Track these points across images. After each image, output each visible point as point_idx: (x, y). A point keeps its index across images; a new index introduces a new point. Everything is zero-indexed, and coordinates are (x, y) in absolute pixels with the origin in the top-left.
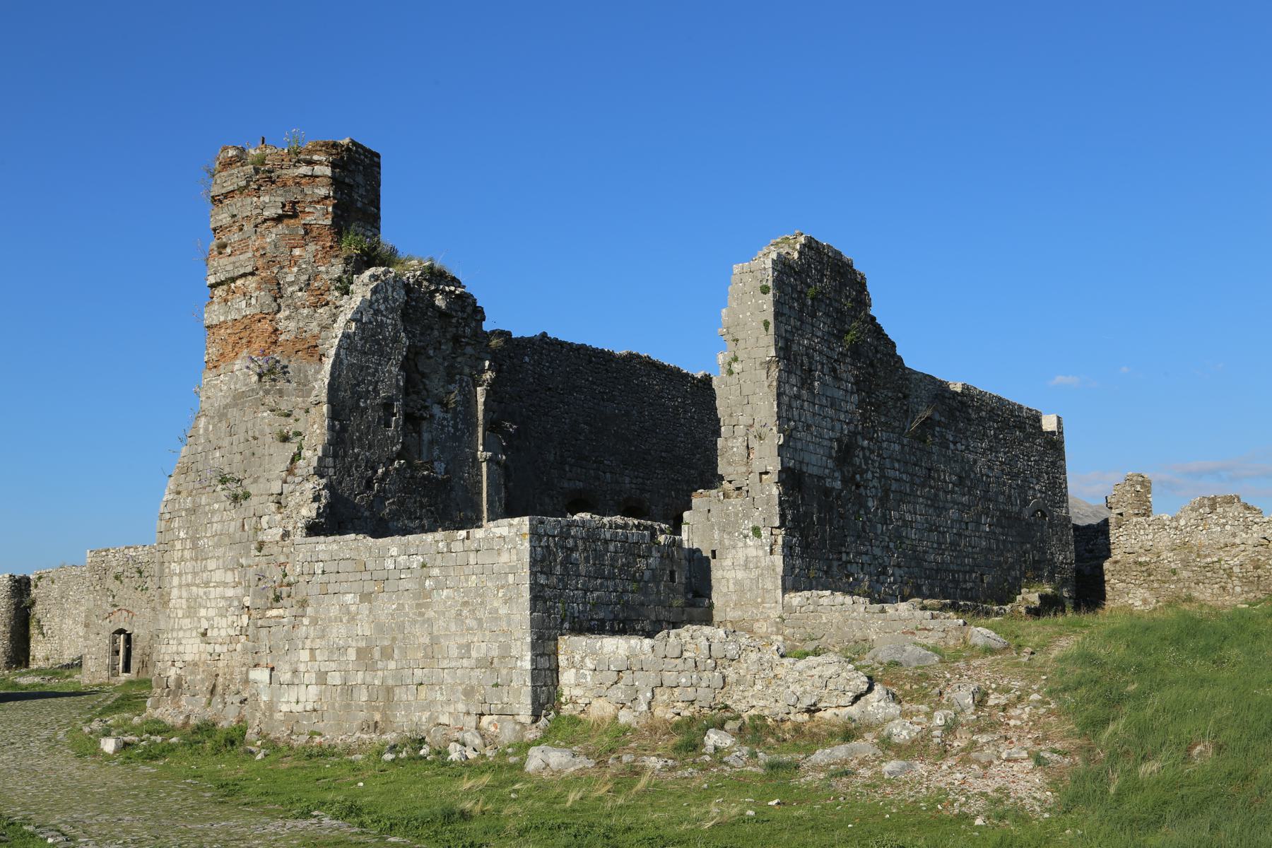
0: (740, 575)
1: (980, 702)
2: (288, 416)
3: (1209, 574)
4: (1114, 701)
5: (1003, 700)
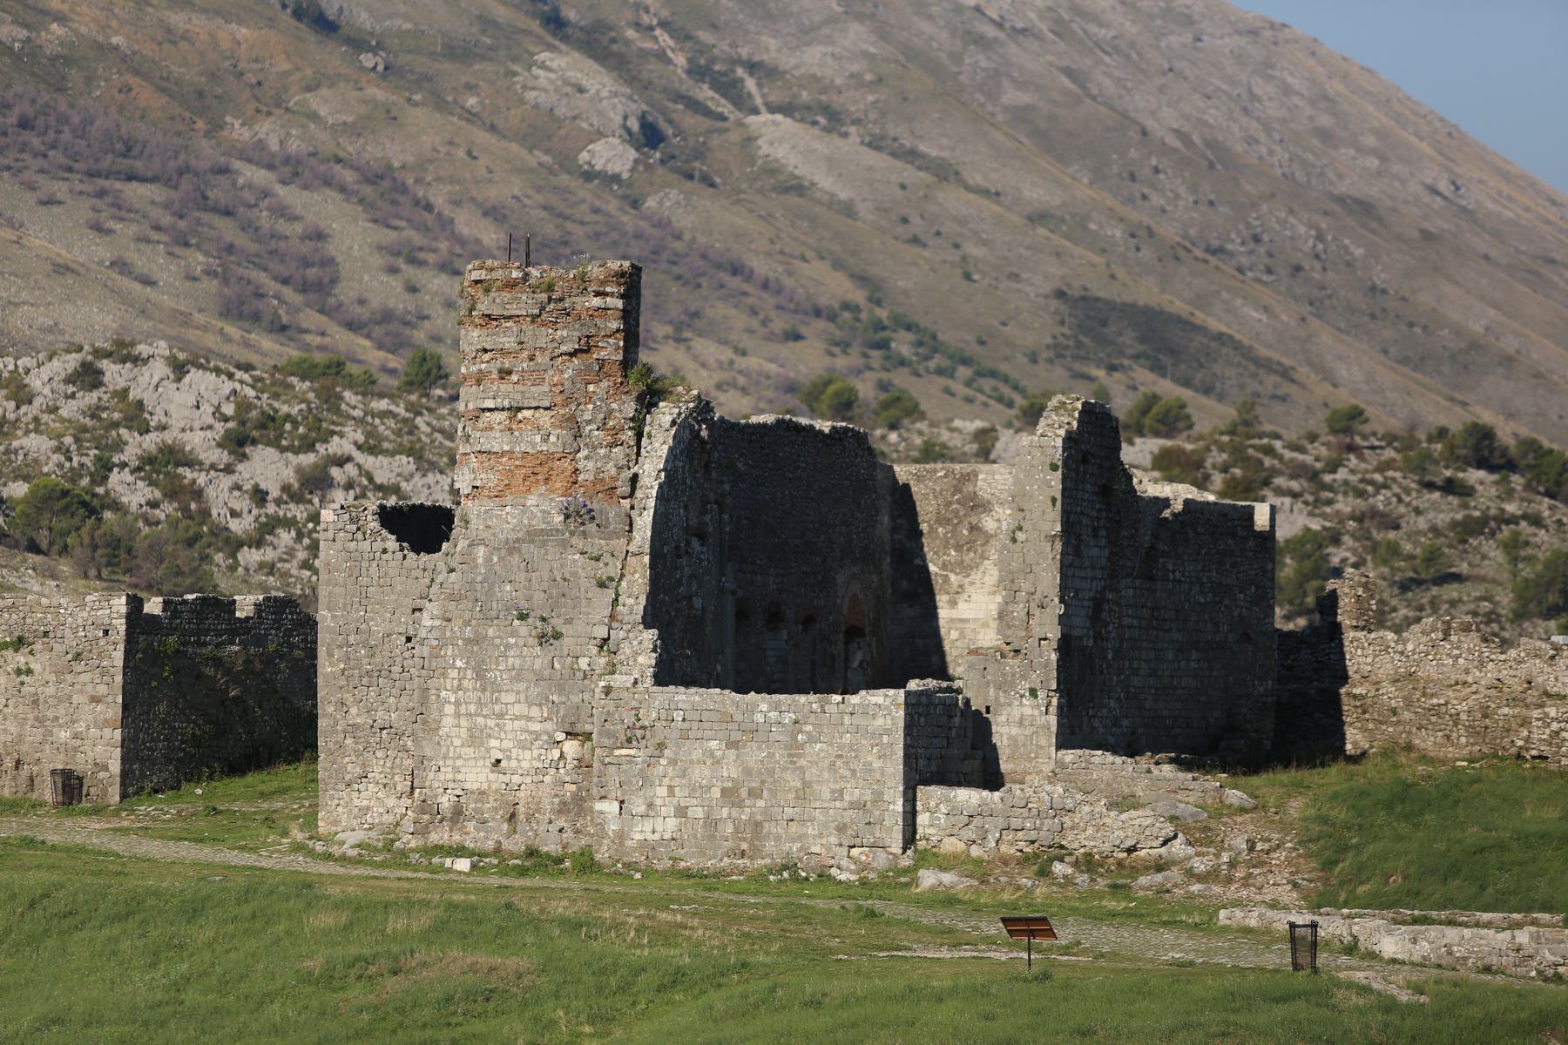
0: (1015, 731)
1: (1251, 849)
2: (598, 559)
3: (1433, 719)
4: (1344, 849)
5: (1267, 846)
